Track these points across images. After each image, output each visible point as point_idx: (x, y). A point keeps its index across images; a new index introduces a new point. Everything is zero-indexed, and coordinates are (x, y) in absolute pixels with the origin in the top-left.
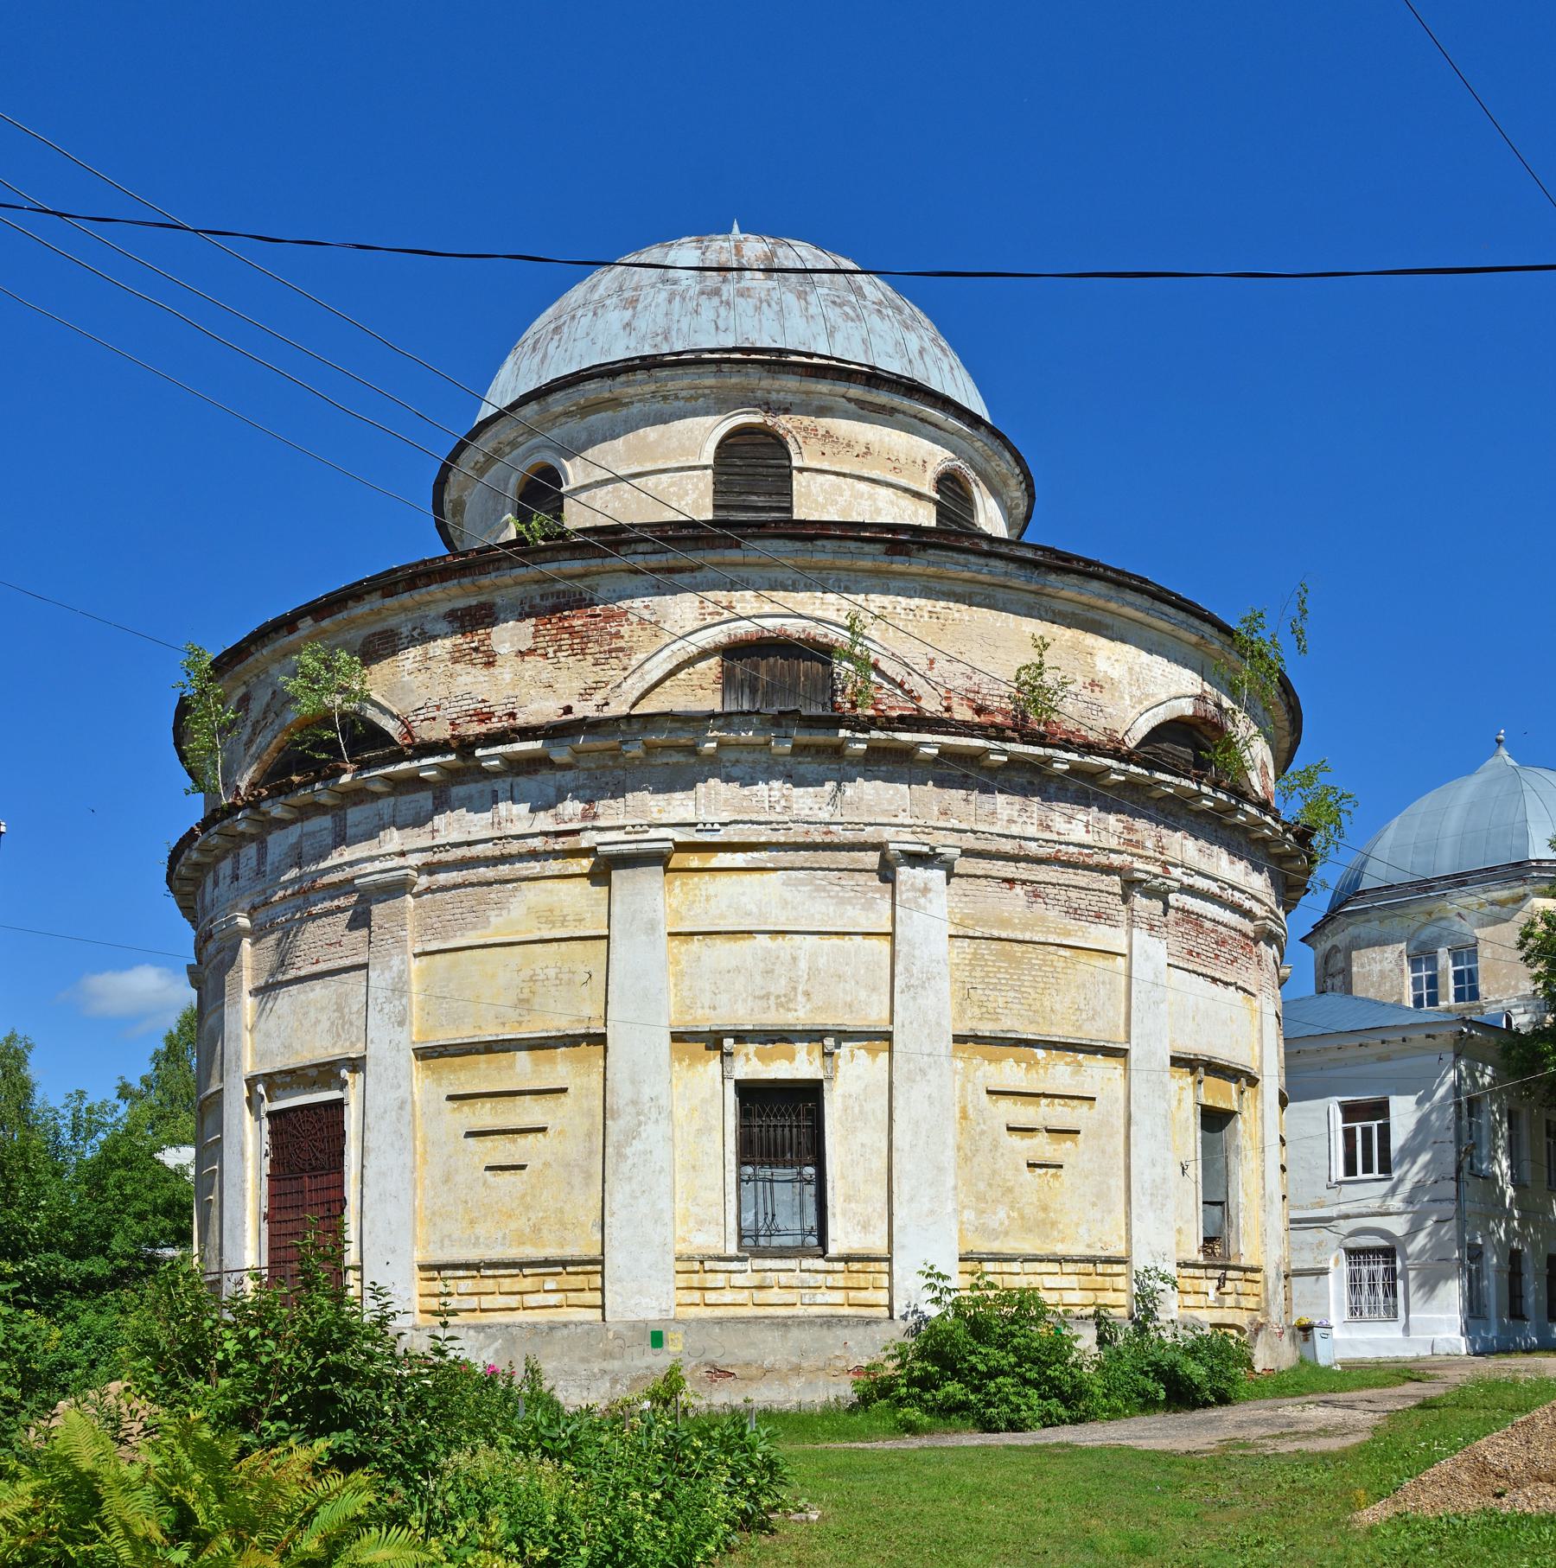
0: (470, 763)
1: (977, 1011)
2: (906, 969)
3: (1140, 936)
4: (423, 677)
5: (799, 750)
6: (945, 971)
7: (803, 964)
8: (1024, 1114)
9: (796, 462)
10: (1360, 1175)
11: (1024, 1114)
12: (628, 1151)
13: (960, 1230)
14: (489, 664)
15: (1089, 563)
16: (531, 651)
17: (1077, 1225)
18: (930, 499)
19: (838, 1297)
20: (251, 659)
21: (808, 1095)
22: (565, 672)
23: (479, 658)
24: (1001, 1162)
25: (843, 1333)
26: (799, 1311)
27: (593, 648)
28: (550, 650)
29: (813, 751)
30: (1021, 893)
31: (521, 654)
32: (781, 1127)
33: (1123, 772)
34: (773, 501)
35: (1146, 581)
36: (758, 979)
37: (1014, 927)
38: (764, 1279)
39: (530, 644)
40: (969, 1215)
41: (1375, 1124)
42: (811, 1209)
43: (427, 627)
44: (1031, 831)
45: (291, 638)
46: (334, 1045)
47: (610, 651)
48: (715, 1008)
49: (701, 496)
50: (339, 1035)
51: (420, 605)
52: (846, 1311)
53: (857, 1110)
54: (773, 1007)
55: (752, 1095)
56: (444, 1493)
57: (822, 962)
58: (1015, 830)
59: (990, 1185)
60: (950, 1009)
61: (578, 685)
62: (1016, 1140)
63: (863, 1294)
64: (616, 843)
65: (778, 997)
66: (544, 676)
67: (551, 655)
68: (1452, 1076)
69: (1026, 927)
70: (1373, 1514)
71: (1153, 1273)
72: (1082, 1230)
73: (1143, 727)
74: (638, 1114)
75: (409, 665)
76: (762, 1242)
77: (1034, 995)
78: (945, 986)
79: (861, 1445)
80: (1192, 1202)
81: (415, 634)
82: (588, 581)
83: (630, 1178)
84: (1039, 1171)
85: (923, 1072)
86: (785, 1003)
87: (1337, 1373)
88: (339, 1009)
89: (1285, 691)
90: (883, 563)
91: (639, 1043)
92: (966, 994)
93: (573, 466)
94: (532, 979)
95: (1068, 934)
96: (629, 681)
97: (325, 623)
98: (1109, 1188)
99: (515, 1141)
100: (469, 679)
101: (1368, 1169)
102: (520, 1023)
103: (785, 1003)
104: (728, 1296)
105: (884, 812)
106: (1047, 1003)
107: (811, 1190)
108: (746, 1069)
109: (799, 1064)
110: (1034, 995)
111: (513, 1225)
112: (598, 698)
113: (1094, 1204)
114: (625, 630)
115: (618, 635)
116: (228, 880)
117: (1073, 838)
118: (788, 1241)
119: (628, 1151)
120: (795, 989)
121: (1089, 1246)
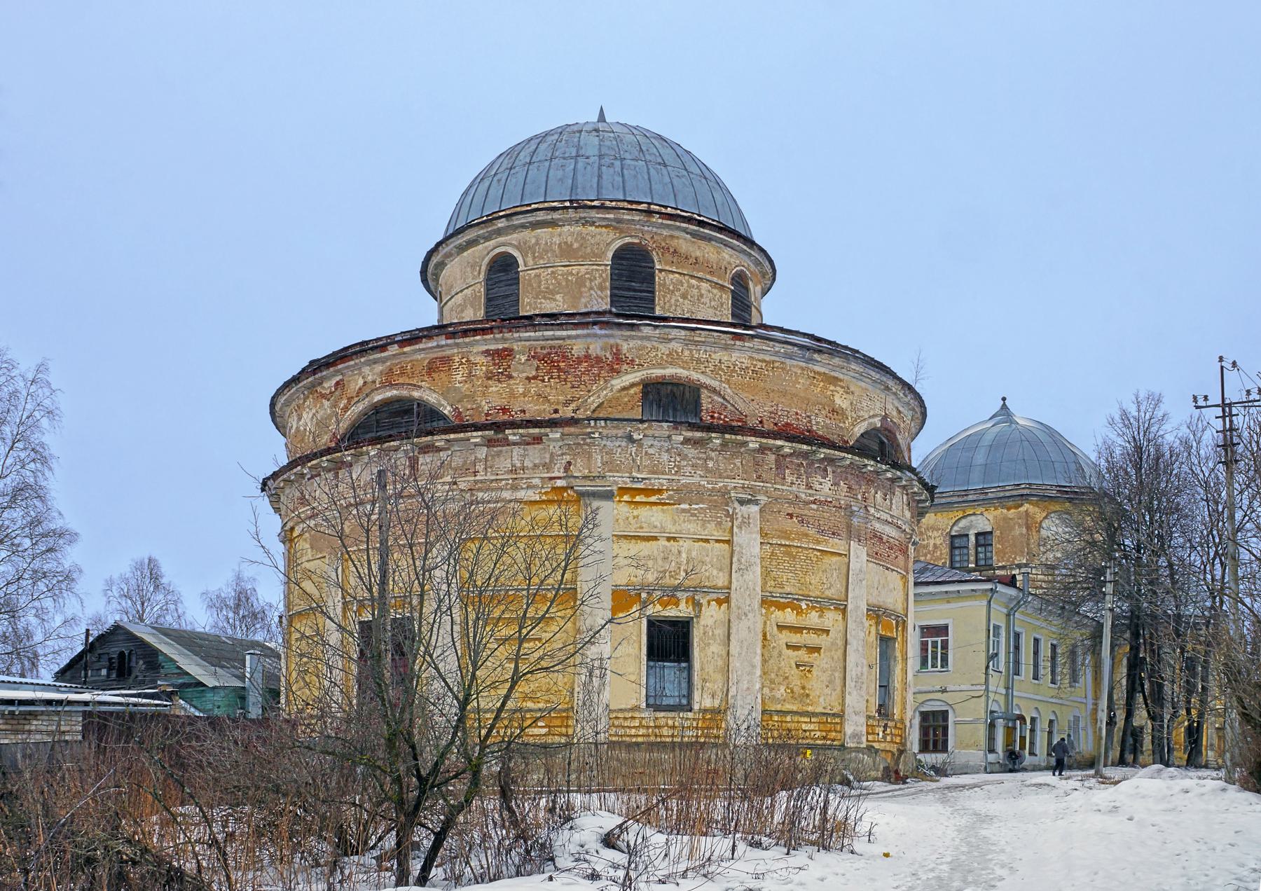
7: (684, 555)
8: (795, 639)
9: (658, 267)
10: (930, 668)
11: (795, 639)
15: (362, 344)
16: (535, 378)
27: (570, 378)
29: (502, 290)
31: (528, 378)
32: (670, 643)
34: (644, 287)
36: (660, 562)
39: (534, 373)
40: (766, 690)
41: (939, 639)
42: (684, 685)
43: (472, 358)
49: (604, 281)
51: (467, 344)
56: (524, 395)
57: (694, 554)
62: (790, 652)
72: (821, 700)
73: (859, 429)
75: (459, 378)
76: (597, 672)
78: (758, 570)
79: (107, 696)
82: (568, 342)
85: (746, 615)
92: (766, 573)
95: (818, 543)
97: (407, 349)
107: (685, 674)
109: (681, 611)
112: (573, 406)
118: (671, 702)
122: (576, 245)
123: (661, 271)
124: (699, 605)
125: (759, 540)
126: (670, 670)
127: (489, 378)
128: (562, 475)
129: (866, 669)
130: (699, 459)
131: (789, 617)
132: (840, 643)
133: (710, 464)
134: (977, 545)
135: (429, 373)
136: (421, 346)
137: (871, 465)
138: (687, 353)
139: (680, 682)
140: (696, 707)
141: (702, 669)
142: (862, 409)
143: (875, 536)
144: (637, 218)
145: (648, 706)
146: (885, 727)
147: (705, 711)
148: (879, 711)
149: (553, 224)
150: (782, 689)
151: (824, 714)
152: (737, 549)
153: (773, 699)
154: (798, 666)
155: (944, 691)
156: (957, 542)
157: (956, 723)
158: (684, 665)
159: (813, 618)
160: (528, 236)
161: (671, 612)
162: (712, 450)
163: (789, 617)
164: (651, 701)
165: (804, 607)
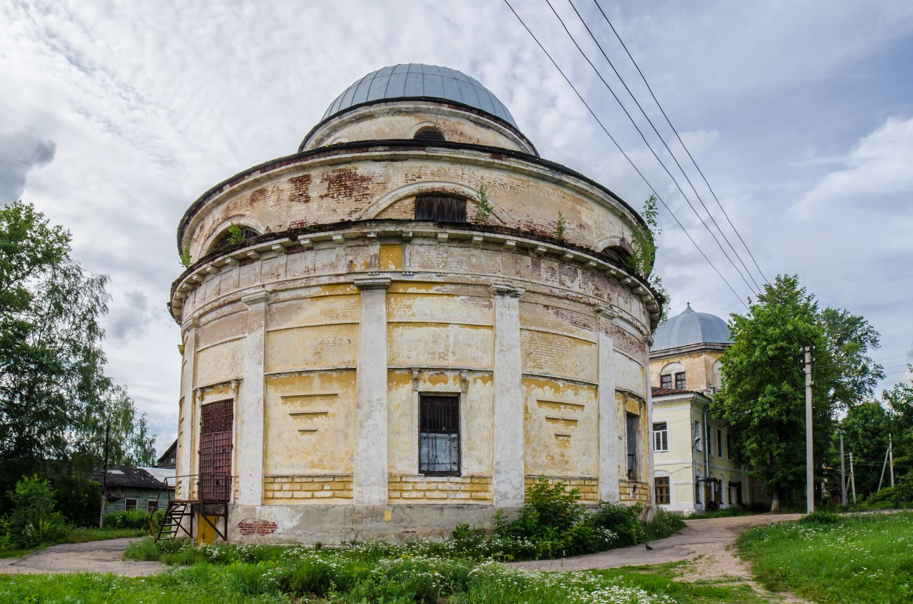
0: (296, 243)
1: (532, 364)
3: (602, 335)
4: (277, 208)
5: (347, 239)
6: (518, 344)
7: (452, 339)
8: (554, 413)
11: (554, 413)
12: (366, 424)
14: (307, 201)
16: (326, 195)
19: (467, 495)
22: (341, 204)
23: (302, 199)
24: (543, 434)
25: (336, 219)
26: (448, 502)
27: (355, 193)
28: (335, 195)
31: (322, 197)
32: (439, 415)
33: (545, 247)
35: (476, 122)
37: (549, 327)
38: (488, 280)
39: (326, 192)
40: (529, 458)
41: (661, 432)
42: (454, 454)
44: (556, 284)
52: (471, 502)
55: (425, 398)
57: (461, 338)
58: (549, 283)
60: (519, 361)
62: (550, 424)
63: (479, 494)
66: (332, 206)
68: (104, 497)
69: (554, 327)
70: (20, 243)
71: (651, 204)
72: (579, 465)
75: (271, 203)
78: (518, 351)
83: (367, 437)
84: (561, 438)
86: (443, 356)
87: (80, 453)
88: (233, 358)
89: (459, 508)
91: (373, 373)
92: (527, 355)
93: (40, 188)
95: (572, 332)
100: (297, 208)
101: (659, 448)
103: (443, 356)
104: (414, 495)
105: (439, 275)
107: (455, 444)
109: (450, 386)
111: (309, 458)
114: (370, 186)
115: (367, 188)
117: (574, 290)
118: (443, 468)
119: (366, 424)
124: (464, 381)
125: (519, 326)
126: (442, 442)
127: (292, 200)
129: (616, 439)
130: (464, 256)
131: (548, 393)
132: (594, 417)
133: (474, 260)
134: (677, 380)
135: (251, 204)
136: (244, 182)
137: (614, 269)
138: (452, 171)
139: (450, 451)
140: (464, 473)
141: (469, 438)
142: (601, 230)
143: (619, 332)
144: (431, 107)
145: (420, 472)
146: (635, 488)
148: (629, 475)
149: (371, 116)
150: (544, 455)
151: (582, 478)
152: (499, 333)
153: (535, 465)
156: (665, 379)
157: (676, 485)
158: (454, 435)
159: (569, 395)
161: (440, 388)
163: (548, 393)
164: (424, 468)
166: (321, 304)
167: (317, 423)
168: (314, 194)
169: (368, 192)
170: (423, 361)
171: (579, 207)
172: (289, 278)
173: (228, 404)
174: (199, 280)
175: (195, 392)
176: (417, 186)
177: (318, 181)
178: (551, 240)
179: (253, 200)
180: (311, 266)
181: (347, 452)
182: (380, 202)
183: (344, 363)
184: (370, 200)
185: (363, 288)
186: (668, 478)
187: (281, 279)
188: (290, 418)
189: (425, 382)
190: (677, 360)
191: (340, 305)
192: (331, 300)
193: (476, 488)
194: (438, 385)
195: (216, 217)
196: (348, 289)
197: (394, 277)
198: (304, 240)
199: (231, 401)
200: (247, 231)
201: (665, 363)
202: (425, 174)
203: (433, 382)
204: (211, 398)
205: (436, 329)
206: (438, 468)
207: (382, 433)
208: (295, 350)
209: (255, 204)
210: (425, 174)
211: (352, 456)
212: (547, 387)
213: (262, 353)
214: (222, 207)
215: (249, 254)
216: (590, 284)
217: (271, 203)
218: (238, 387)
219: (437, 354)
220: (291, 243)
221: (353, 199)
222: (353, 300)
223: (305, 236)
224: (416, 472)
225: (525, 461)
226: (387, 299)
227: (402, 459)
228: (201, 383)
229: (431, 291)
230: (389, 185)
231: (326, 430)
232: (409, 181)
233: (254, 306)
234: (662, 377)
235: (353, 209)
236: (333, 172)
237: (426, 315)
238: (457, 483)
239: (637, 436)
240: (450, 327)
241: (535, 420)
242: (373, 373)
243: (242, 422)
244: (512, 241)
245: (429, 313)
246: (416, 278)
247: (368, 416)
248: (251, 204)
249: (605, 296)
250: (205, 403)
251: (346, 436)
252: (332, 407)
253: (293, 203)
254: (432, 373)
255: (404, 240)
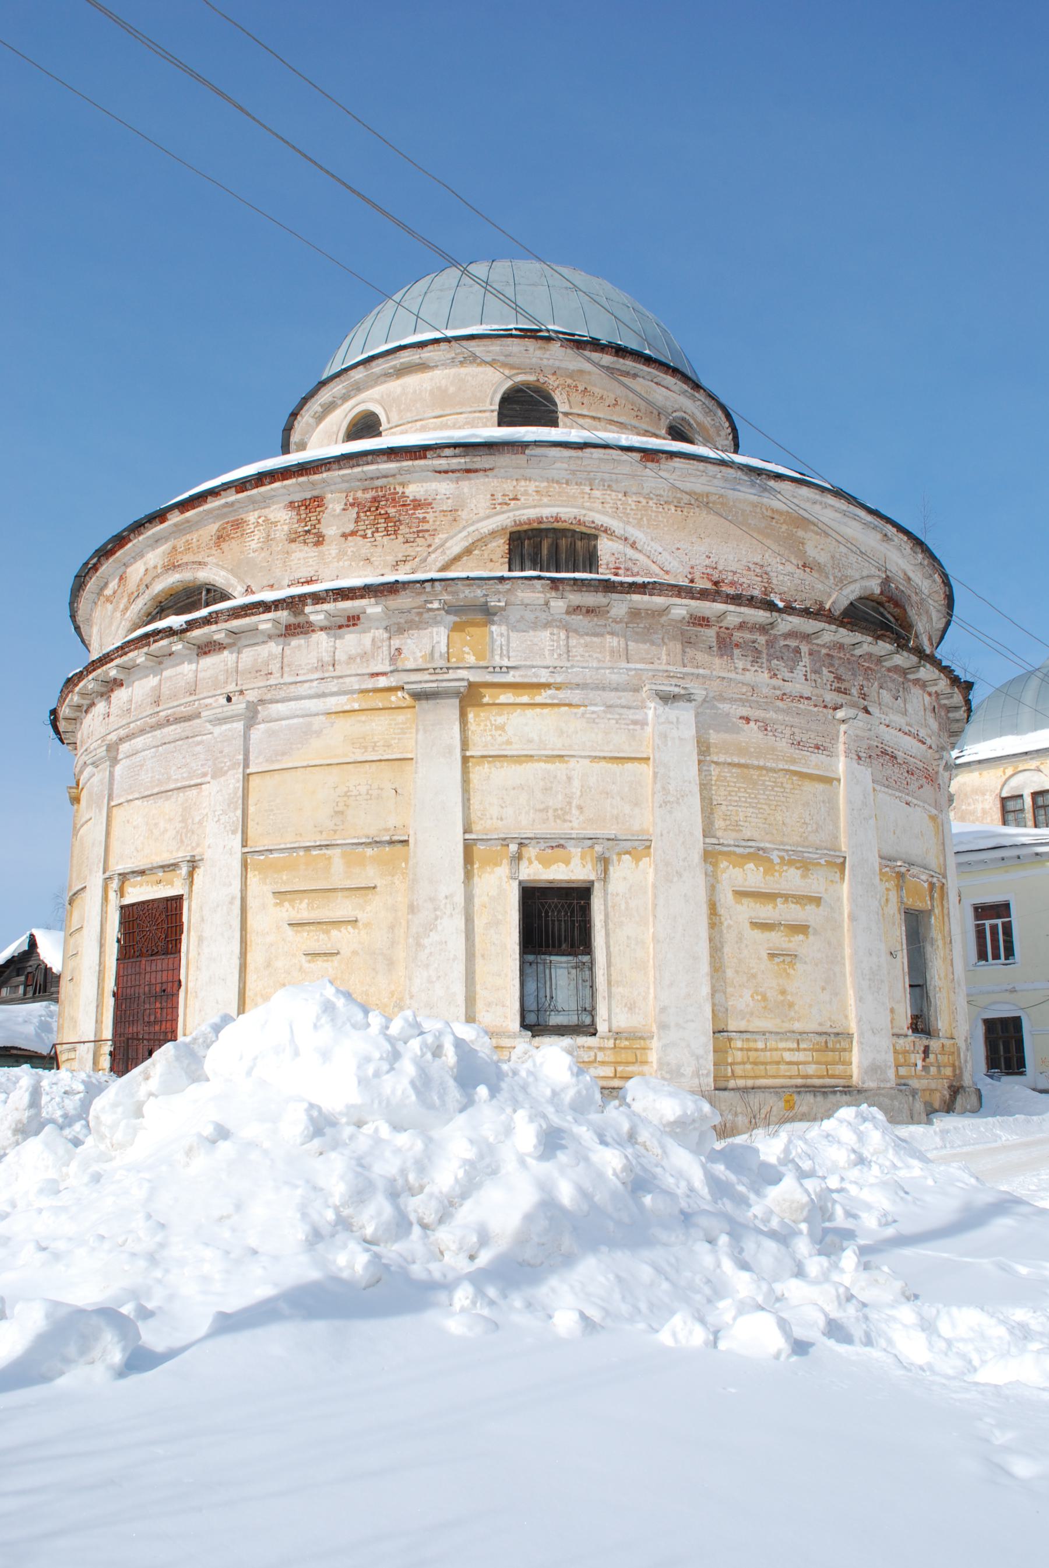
2: (664, 788)
5: (635, 614)
7: (576, 783)
8: (766, 912)
11: (766, 912)
12: (426, 941)
13: (713, 1011)
16: (353, 533)
17: (810, 1006)
18: (809, 1195)
20: (130, 545)
21: (577, 898)
22: (379, 549)
23: (311, 538)
27: (404, 529)
28: (369, 532)
30: (756, 727)
31: (345, 536)
39: (351, 527)
41: (999, 922)
45: (162, 526)
46: (178, 849)
47: (418, 532)
48: (502, 819)
50: (182, 842)
53: (623, 907)
54: (551, 818)
59: (737, 972)
61: (391, 559)
62: (757, 934)
64: (420, 682)
65: (556, 810)
66: (363, 551)
67: (369, 535)
74: (435, 910)
75: (254, 545)
77: (768, 811)
80: (900, 986)
81: (260, 521)
83: (427, 966)
86: (561, 815)
88: (184, 820)
90: (183, 988)
94: (347, 795)
95: (793, 761)
96: (433, 556)
98: (835, 974)
99: (327, 932)
101: (996, 956)
102: (335, 831)
103: (561, 815)
106: (779, 818)
108: (527, 871)
110: (768, 811)
113: (823, 989)
114: (430, 517)
115: (424, 520)
116: (101, 717)
119: (426, 941)
120: (570, 803)
121: (820, 1024)
122: (452, 390)
123: (566, 414)
126: (561, 970)
127: (293, 541)
128: (388, 669)
135: (218, 545)
140: (602, 1027)
147: (617, 1035)
149: (423, 367)
150: (747, 994)
154: (772, 956)
155: (1013, 991)
156: (1011, 805)
159: (792, 880)
160: (395, 386)
162: (615, 621)
164: (531, 1019)
165: (777, 860)
166: (345, 726)
167: (343, 938)
168: (331, 530)
169: (426, 526)
170: (526, 824)
171: (801, 533)
172: (287, 679)
173: (172, 907)
174: (120, 677)
175: (107, 880)
176: (511, 514)
177: (338, 508)
178: (751, 602)
179: (221, 538)
180: (327, 658)
181: (392, 993)
182: (448, 545)
183: (387, 830)
184: (430, 540)
185: (419, 696)
186: (1016, 1022)
187: (272, 681)
188: (289, 932)
189: (530, 862)
190: (1033, 764)
191: (379, 726)
192: (363, 717)
193: (624, 1056)
194: (554, 867)
195: (152, 564)
196: (393, 698)
197: (475, 677)
198: (316, 614)
199: (179, 899)
200: (208, 591)
201: (1010, 771)
202: (526, 493)
203: (546, 863)
204: (138, 893)
205: (549, 766)
206: (555, 1020)
207: (455, 958)
208: (296, 808)
209: (224, 546)
210: (526, 493)
211: (401, 999)
212: (751, 866)
213: (239, 813)
214: (165, 548)
215: (216, 637)
216: (825, 670)
217: (254, 545)
218: (191, 875)
219: (551, 811)
220: (293, 620)
221: (401, 539)
222: (401, 717)
223: (318, 607)
224: (515, 1024)
225: (714, 1005)
226: (463, 715)
227: (489, 1005)
228: (119, 866)
229: (539, 699)
230: (463, 514)
231: (355, 953)
232: (499, 504)
233: (224, 727)
234: (1004, 800)
235: (400, 557)
236: (364, 490)
237: (530, 741)
238: (590, 1048)
239: (929, 949)
240: (573, 762)
241: (729, 927)
242: (439, 847)
243: (201, 939)
244: (681, 608)
245: (536, 738)
246: (510, 678)
247: (430, 927)
248: (218, 545)
249: (854, 691)
250: (128, 900)
251: (391, 963)
252: (372, 910)
253: (293, 545)
254: (543, 845)
255: (487, 614)
